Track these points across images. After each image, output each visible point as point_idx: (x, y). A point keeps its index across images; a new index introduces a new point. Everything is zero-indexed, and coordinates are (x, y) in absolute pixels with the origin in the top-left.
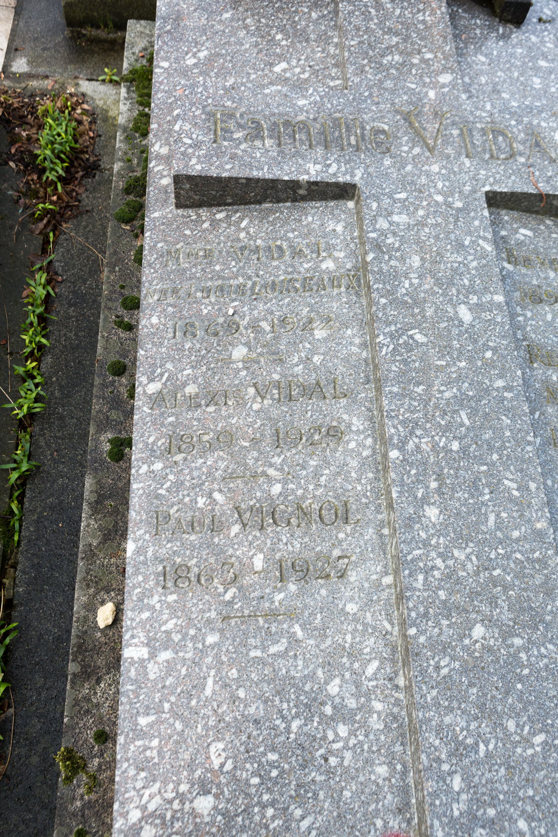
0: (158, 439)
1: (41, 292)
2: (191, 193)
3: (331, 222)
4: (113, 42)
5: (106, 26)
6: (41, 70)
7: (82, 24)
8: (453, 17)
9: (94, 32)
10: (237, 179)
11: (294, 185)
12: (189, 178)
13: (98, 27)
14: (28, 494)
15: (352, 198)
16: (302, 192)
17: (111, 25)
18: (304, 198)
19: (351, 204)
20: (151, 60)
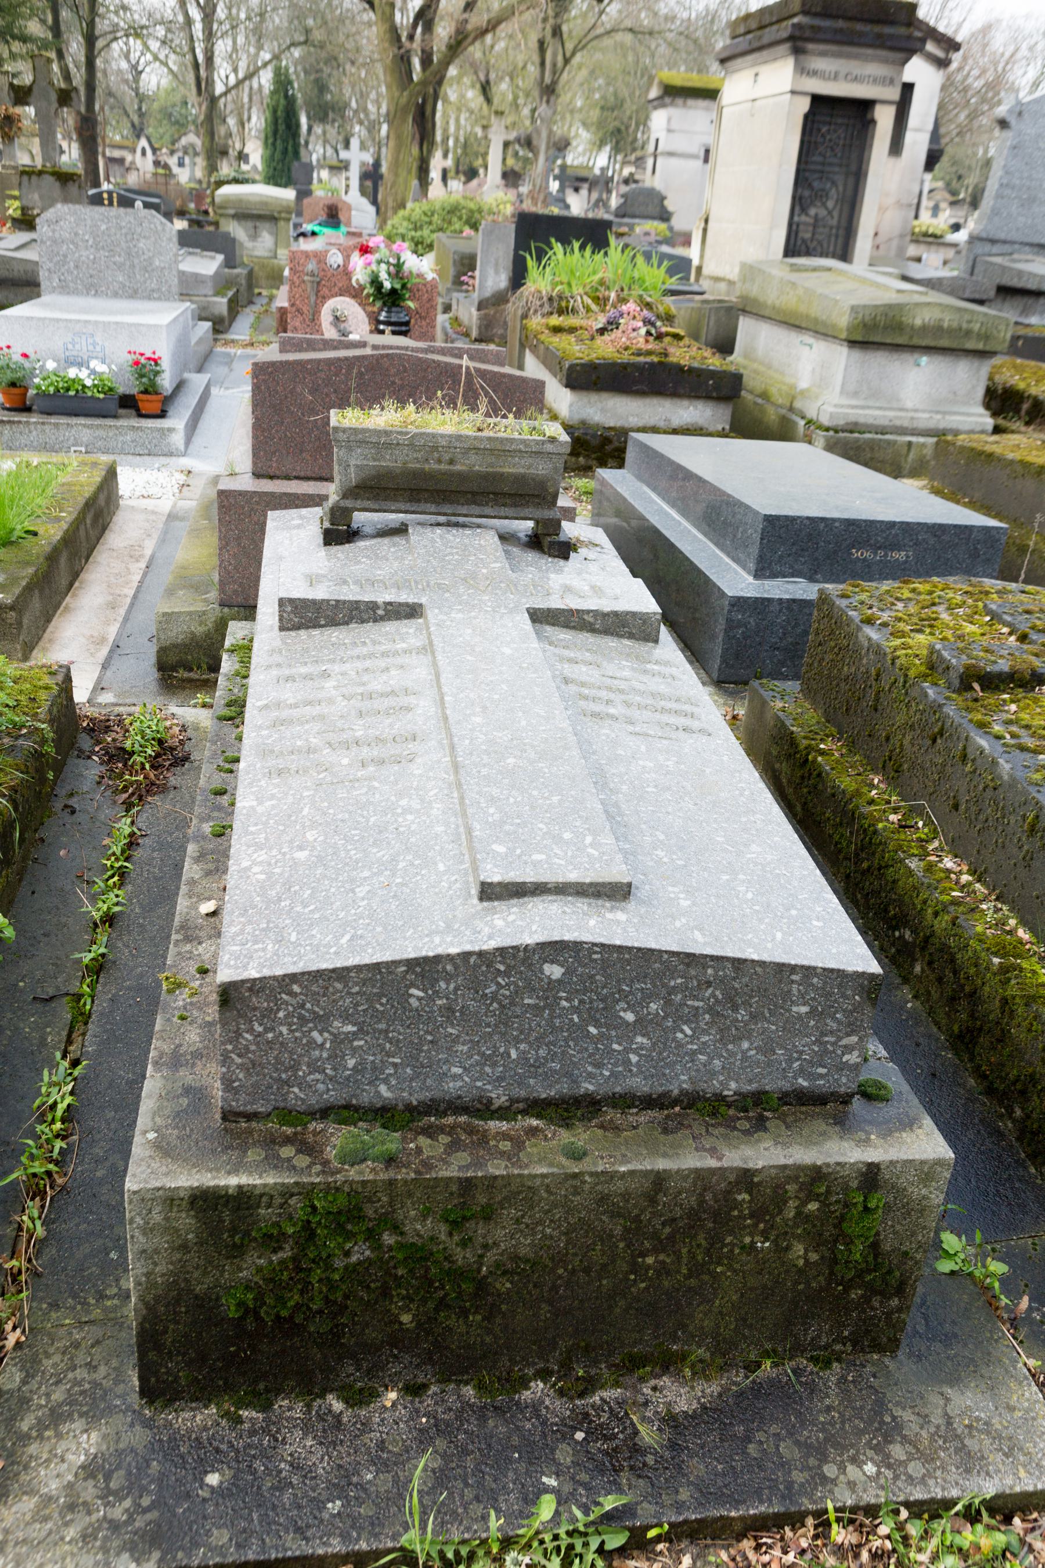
0: (261, 873)
1: (127, 830)
2: (292, 616)
3: (407, 627)
4: (207, 681)
5: (199, 667)
6: (263, 338)
7: (174, 669)
8: (506, 552)
9: (186, 675)
10: (328, 601)
11: (373, 606)
12: (291, 601)
13: (191, 670)
14: (101, 980)
15: (421, 616)
16: (380, 612)
17: (205, 667)
18: (382, 619)
19: (420, 621)
20: (251, 640)
